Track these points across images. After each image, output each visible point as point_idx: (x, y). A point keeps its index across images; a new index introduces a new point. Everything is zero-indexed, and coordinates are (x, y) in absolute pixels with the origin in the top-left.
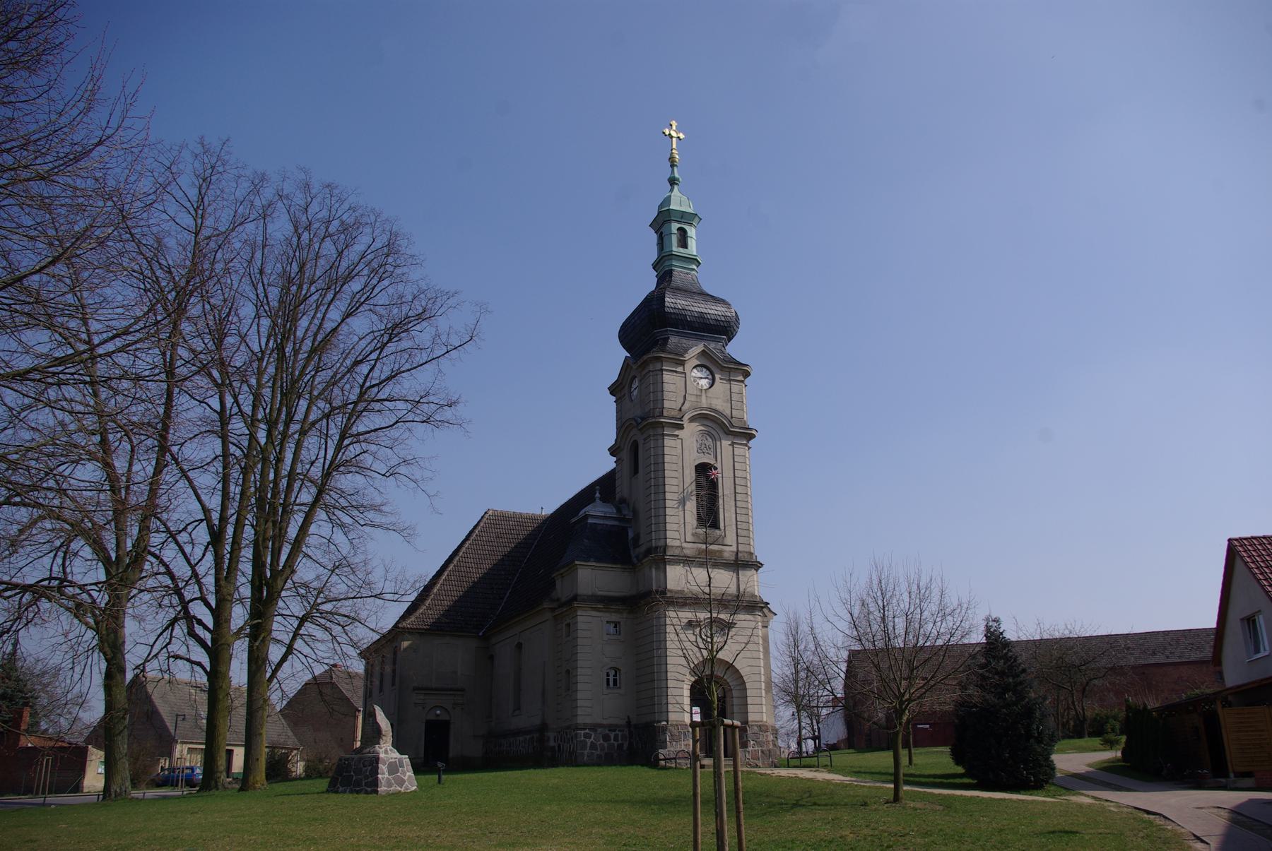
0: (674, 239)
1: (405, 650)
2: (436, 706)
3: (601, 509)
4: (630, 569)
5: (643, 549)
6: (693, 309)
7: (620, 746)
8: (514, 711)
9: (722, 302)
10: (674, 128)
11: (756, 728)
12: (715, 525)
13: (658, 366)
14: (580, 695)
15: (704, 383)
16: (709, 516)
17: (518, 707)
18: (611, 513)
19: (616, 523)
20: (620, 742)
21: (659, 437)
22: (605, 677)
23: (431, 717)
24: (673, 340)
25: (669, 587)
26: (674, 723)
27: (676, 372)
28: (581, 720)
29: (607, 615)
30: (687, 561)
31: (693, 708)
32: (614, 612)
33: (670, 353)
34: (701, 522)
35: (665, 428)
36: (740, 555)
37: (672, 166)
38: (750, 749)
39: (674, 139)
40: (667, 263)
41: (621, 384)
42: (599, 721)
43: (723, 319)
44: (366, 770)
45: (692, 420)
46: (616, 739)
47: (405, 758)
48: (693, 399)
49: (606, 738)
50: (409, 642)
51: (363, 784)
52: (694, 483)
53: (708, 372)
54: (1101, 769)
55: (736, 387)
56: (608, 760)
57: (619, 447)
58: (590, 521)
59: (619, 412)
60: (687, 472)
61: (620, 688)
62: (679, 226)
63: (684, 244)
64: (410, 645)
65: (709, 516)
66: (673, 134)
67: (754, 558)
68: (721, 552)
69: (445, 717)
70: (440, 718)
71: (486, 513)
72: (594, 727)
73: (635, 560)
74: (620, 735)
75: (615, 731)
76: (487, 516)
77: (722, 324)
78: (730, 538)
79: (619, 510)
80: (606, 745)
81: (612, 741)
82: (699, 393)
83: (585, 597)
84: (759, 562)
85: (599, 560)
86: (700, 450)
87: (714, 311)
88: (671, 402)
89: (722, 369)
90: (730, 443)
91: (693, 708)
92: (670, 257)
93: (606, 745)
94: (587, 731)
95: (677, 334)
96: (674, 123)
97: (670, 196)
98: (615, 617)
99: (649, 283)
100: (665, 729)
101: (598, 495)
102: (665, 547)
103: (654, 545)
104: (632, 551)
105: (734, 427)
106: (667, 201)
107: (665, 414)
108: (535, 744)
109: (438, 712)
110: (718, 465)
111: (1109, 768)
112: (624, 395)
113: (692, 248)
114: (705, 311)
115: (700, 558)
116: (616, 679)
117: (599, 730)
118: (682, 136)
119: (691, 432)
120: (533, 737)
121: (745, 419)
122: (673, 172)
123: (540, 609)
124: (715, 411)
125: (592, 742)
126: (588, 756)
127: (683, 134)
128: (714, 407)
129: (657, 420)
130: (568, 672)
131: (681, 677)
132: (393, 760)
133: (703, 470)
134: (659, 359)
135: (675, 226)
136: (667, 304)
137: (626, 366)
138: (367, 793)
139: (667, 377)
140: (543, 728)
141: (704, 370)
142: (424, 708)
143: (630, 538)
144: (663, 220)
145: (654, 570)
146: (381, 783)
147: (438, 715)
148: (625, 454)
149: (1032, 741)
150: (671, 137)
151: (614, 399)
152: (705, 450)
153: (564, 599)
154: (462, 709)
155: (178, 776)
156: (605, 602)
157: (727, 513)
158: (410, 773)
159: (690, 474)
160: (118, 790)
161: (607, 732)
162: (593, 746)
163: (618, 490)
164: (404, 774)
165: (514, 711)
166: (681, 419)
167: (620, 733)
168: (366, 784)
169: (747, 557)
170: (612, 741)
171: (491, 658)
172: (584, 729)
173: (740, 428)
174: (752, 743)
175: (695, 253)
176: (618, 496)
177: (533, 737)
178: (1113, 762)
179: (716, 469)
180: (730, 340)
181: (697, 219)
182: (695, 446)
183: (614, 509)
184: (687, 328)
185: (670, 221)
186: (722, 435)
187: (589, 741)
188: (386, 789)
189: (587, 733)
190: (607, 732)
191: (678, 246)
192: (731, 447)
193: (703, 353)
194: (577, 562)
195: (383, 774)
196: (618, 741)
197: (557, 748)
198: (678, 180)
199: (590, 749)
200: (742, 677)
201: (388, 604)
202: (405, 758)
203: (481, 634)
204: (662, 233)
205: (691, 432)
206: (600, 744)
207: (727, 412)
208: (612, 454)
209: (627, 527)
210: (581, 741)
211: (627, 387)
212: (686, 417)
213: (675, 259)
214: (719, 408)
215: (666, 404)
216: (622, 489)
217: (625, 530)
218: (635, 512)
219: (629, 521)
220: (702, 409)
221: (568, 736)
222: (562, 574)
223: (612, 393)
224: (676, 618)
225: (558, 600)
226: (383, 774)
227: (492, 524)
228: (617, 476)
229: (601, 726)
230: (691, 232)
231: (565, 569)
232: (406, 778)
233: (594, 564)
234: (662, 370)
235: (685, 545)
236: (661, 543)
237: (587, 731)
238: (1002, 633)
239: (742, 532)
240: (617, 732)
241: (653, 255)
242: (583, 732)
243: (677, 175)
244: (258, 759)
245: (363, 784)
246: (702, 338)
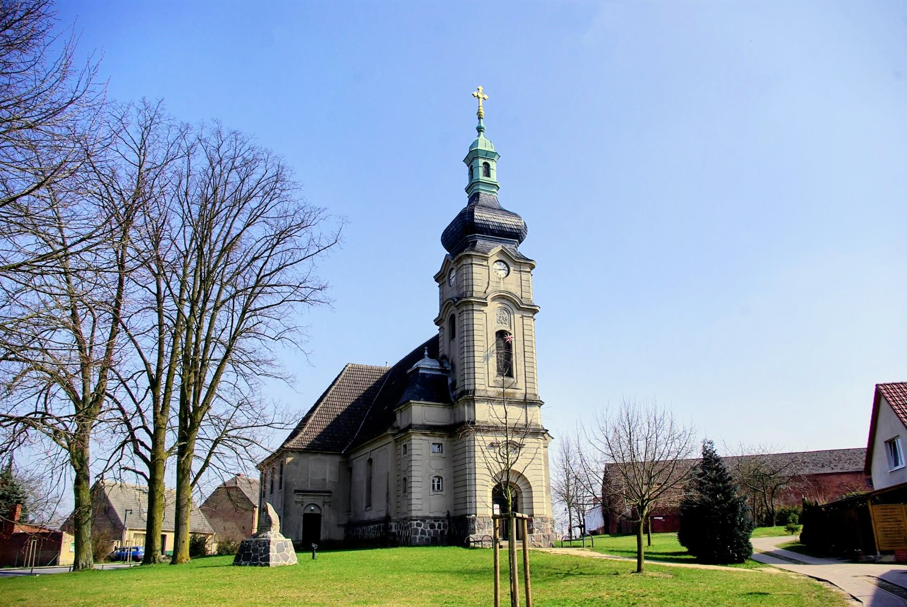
1: (289, 463)
5: (459, 391)
6: (494, 220)
7: (442, 532)
9: (516, 215)
10: (481, 91)
11: (539, 519)
12: (510, 375)
13: (469, 261)
14: (414, 496)
15: (503, 273)
16: (506, 368)
19: (439, 373)
20: (442, 529)
21: (470, 312)
23: (308, 511)
24: (480, 242)
25: (477, 419)
26: (481, 516)
27: (482, 265)
28: (414, 514)
30: (489, 400)
33: (478, 252)
34: (500, 372)
35: (474, 305)
37: (480, 118)
38: (535, 534)
39: (481, 100)
40: (475, 188)
41: (443, 273)
42: (427, 514)
43: (515, 227)
45: (494, 299)
46: (439, 527)
48: (494, 284)
49: (432, 526)
50: (292, 458)
52: (495, 345)
53: (505, 266)
54: (787, 549)
55: (525, 276)
56: (434, 542)
58: (421, 371)
61: (442, 490)
64: (293, 460)
65: (506, 368)
66: (480, 95)
68: (514, 394)
69: (317, 512)
70: (313, 512)
72: (423, 519)
75: (438, 521)
77: (515, 231)
78: (521, 384)
79: (441, 364)
81: (437, 529)
82: (498, 281)
86: (499, 321)
87: (508, 222)
88: (479, 288)
89: (515, 263)
90: (520, 316)
94: (419, 521)
95: (483, 238)
96: (480, 88)
97: (478, 140)
100: (474, 520)
103: (466, 389)
106: (476, 143)
107: (474, 295)
109: (313, 508)
110: (512, 332)
111: (792, 548)
112: (445, 282)
114: (503, 222)
117: (427, 521)
118: (486, 97)
119: (493, 307)
124: (510, 293)
126: (419, 539)
128: (509, 290)
130: (405, 479)
131: (486, 483)
132: (280, 542)
133: (501, 334)
134: (470, 256)
135: (481, 162)
136: (475, 217)
137: (446, 262)
139: (476, 269)
140: (387, 519)
141: (502, 264)
142: (302, 505)
144: (472, 157)
145: (466, 407)
147: (312, 510)
148: (446, 325)
149: (736, 528)
150: (479, 98)
151: (438, 284)
152: (502, 321)
154: (330, 506)
155: (127, 554)
156: (431, 429)
157: (518, 366)
158: (293, 551)
159: (492, 338)
160: (84, 564)
161: (433, 522)
162: (423, 532)
164: (288, 552)
166: (485, 299)
167: (442, 523)
169: (532, 398)
170: (437, 529)
173: (528, 305)
174: (536, 530)
178: (793, 543)
179: (510, 334)
180: (520, 242)
181: (497, 156)
182: (496, 318)
185: (478, 157)
188: (275, 562)
190: (433, 522)
192: (521, 319)
193: (502, 252)
194: (411, 401)
198: (483, 128)
205: (493, 307)
207: (519, 295)
210: (414, 529)
212: (489, 298)
214: (513, 291)
215: (475, 288)
219: (448, 372)
220: (500, 291)
224: (481, 441)
227: (350, 373)
229: (428, 518)
230: (493, 165)
232: (289, 555)
235: (488, 389)
236: (471, 387)
237: (419, 521)
238: (714, 452)
241: (466, 182)
242: (415, 522)
243: (482, 125)
244: (184, 542)
246: (501, 241)
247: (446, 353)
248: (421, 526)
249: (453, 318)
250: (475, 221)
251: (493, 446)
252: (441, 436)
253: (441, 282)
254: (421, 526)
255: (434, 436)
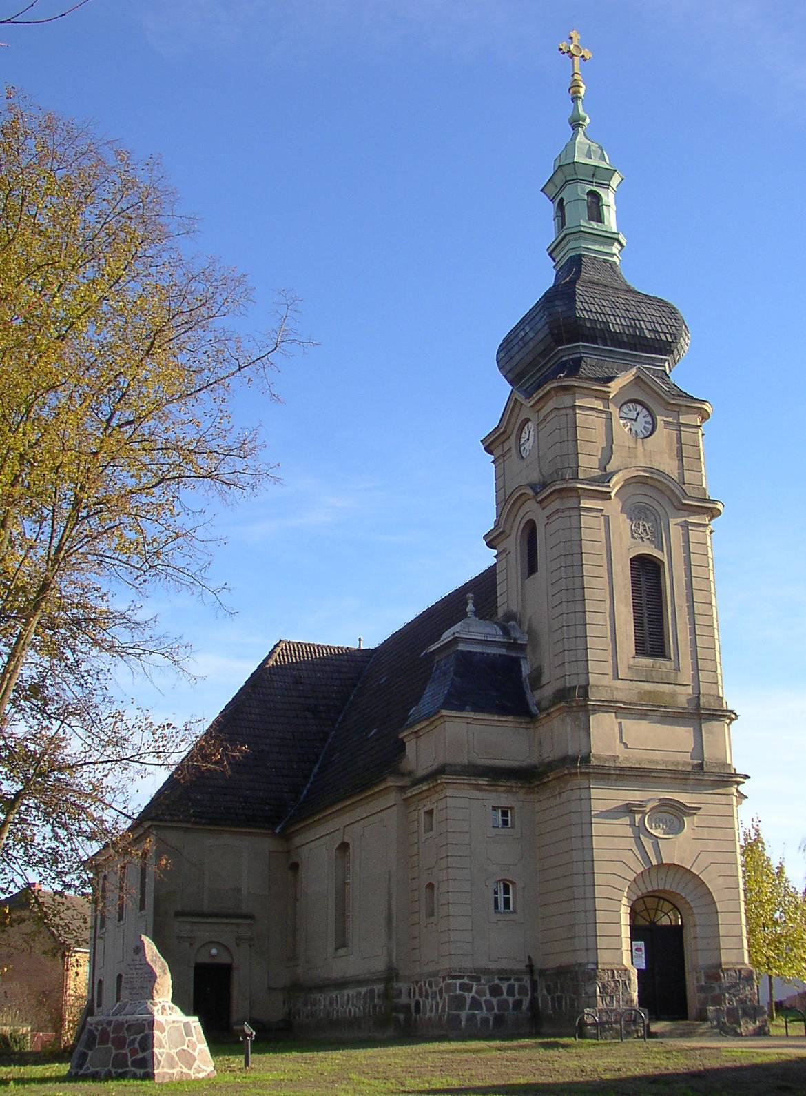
0: (583, 208)
2: (212, 942)
3: (480, 629)
4: (528, 723)
5: (548, 691)
7: (517, 1005)
8: (336, 949)
17: (342, 943)
18: (495, 636)
20: (517, 997)
21: (573, 513)
22: (492, 896)
23: (203, 959)
29: (493, 795)
30: (623, 710)
31: (633, 943)
32: (505, 792)
34: (641, 651)
35: (581, 497)
36: (702, 700)
39: (576, 59)
42: (484, 963)
44: (134, 1040)
46: (511, 991)
47: (194, 1022)
49: (496, 991)
51: (129, 1063)
57: (503, 532)
58: (462, 647)
59: (500, 477)
60: (616, 568)
61: (514, 912)
62: (589, 188)
63: (595, 209)
67: (725, 705)
68: (673, 695)
69: (225, 959)
70: (216, 960)
71: (276, 646)
73: (534, 709)
74: (516, 987)
75: (509, 979)
76: (278, 650)
78: (686, 675)
79: (506, 632)
80: (495, 1001)
81: (505, 996)
83: (459, 768)
84: (731, 711)
85: (477, 708)
91: (633, 943)
92: (577, 235)
93: (495, 1001)
94: (466, 980)
98: (504, 800)
99: (545, 278)
101: (470, 607)
102: (585, 689)
104: (528, 696)
105: (689, 498)
106: (570, 147)
107: (581, 476)
108: (376, 1000)
109: (214, 951)
112: (510, 450)
113: (610, 223)
115: (642, 705)
116: (509, 898)
120: (372, 991)
121: (704, 486)
122: (576, 107)
123: (307, 823)
125: (473, 998)
127: (591, 51)
129: (571, 485)
130: (430, 886)
134: (566, 389)
137: (512, 407)
138: (135, 1077)
140: (391, 975)
142: (191, 944)
143: (524, 675)
146: (159, 1062)
147: (213, 956)
148: (514, 543)
153: (421, 772)
154: (250, 946)
161: (497, 981)
162: (475, 1004)
163: (500, 600)
165: (336, 949)
167: (517, 984)
168: (135, 1063)
170: (505, 996)
171: (295, 867)
172: (461, 977)
175: (615, 230)
176: (501, 612)
177: (372, 991)
183: (498, 629)
184: (610, 344)
186: (669, 509)
187: (468, 996)
189: (465, 984)
190: (497, 981)
191: (590, 219)
195: (161, 1046)
196: (514, 996)
197: (413, 1009)
199: (470, 1009)
200: (710, 893)
201: (150, 768)
202: (194, 1022)
203: (277, 831)
204: (562, 200)
206: (485, 1001)
207: (675, 475)
208: (490, 545)
209: (520, 658)
211: (513, 438)
213: (583, 238)
216: (507, 600)
217: (516, 663)
218: (531, 633)
219: (522, 647)
221: (434, 988)
222: (417, 732)
223: (488, 450)
225: (410, 773)
226: (161, 1046)
228: (499, 579)
229: (487, 972)
230: (609, 197)
231: (424, 724)
232: (196, 1054)
233: (471, 714)
234: (574, 407)
235: (619, 684)
236: (578, 681)
239: (703, 664)
240: (512, 981)
241: (549, 235)
242: (458, 982)
245: (129, 1063)
246: (635, 360)
247: (514, 608)
248: (469, 989)
249: (530, 533)
250: (579, 314)
251: (631, 811)
252: (509, 791)
253: (498, 452)
254: (469, 989)
255: (496, 791)
